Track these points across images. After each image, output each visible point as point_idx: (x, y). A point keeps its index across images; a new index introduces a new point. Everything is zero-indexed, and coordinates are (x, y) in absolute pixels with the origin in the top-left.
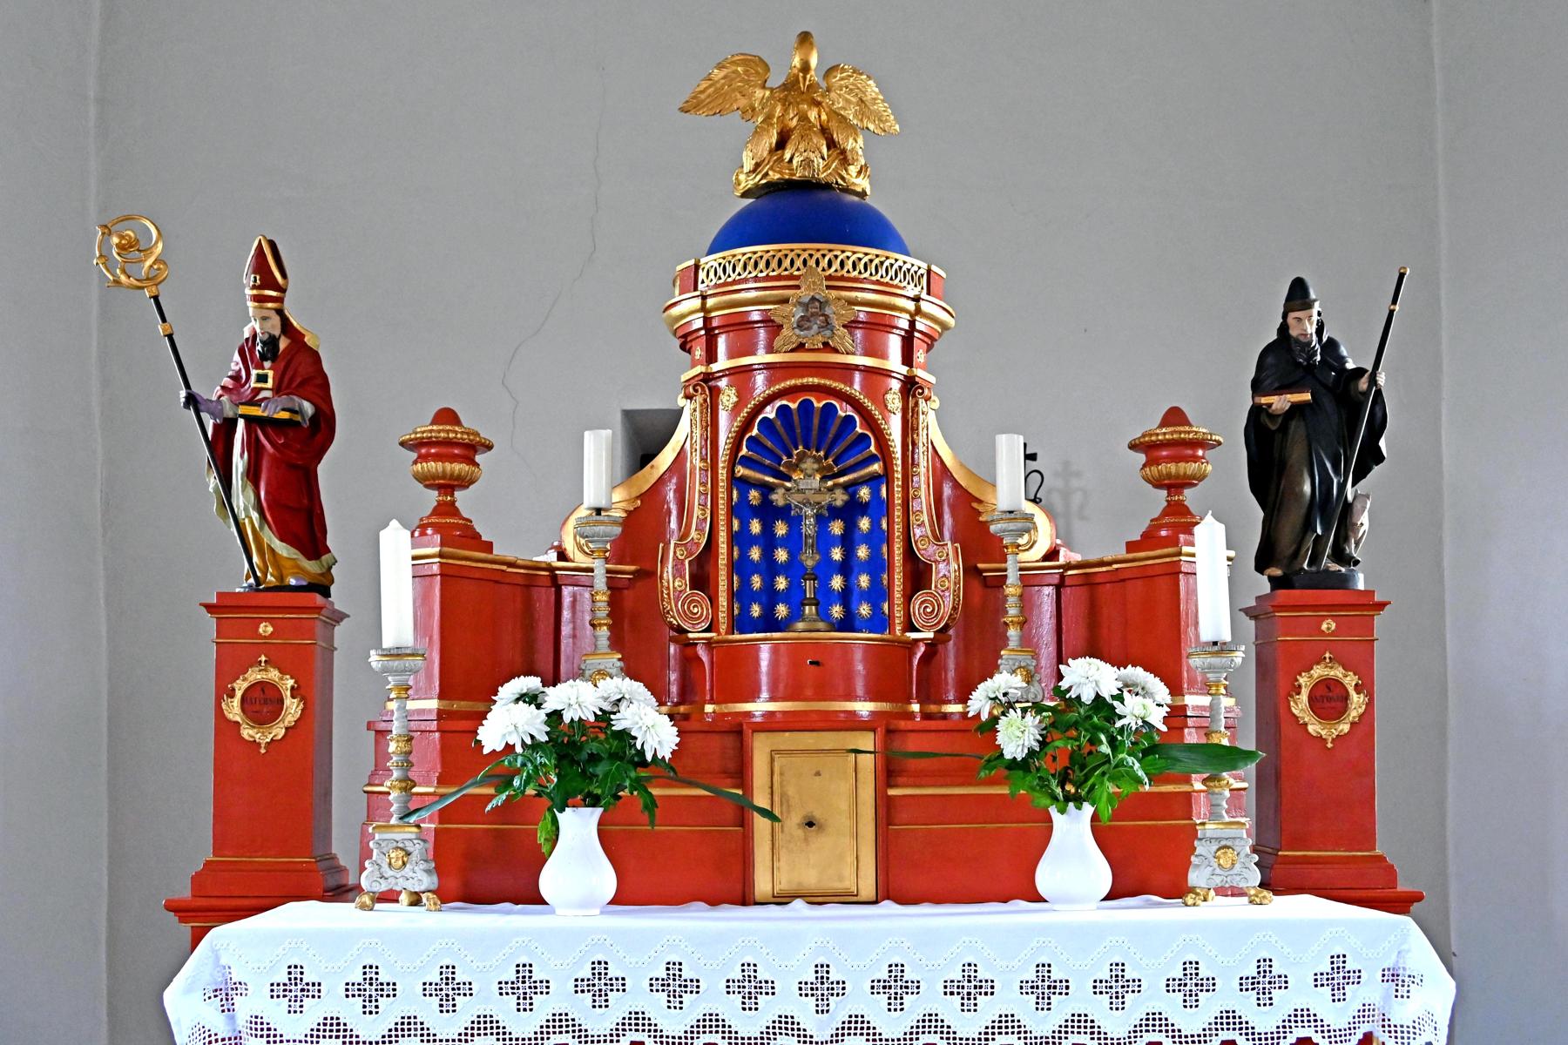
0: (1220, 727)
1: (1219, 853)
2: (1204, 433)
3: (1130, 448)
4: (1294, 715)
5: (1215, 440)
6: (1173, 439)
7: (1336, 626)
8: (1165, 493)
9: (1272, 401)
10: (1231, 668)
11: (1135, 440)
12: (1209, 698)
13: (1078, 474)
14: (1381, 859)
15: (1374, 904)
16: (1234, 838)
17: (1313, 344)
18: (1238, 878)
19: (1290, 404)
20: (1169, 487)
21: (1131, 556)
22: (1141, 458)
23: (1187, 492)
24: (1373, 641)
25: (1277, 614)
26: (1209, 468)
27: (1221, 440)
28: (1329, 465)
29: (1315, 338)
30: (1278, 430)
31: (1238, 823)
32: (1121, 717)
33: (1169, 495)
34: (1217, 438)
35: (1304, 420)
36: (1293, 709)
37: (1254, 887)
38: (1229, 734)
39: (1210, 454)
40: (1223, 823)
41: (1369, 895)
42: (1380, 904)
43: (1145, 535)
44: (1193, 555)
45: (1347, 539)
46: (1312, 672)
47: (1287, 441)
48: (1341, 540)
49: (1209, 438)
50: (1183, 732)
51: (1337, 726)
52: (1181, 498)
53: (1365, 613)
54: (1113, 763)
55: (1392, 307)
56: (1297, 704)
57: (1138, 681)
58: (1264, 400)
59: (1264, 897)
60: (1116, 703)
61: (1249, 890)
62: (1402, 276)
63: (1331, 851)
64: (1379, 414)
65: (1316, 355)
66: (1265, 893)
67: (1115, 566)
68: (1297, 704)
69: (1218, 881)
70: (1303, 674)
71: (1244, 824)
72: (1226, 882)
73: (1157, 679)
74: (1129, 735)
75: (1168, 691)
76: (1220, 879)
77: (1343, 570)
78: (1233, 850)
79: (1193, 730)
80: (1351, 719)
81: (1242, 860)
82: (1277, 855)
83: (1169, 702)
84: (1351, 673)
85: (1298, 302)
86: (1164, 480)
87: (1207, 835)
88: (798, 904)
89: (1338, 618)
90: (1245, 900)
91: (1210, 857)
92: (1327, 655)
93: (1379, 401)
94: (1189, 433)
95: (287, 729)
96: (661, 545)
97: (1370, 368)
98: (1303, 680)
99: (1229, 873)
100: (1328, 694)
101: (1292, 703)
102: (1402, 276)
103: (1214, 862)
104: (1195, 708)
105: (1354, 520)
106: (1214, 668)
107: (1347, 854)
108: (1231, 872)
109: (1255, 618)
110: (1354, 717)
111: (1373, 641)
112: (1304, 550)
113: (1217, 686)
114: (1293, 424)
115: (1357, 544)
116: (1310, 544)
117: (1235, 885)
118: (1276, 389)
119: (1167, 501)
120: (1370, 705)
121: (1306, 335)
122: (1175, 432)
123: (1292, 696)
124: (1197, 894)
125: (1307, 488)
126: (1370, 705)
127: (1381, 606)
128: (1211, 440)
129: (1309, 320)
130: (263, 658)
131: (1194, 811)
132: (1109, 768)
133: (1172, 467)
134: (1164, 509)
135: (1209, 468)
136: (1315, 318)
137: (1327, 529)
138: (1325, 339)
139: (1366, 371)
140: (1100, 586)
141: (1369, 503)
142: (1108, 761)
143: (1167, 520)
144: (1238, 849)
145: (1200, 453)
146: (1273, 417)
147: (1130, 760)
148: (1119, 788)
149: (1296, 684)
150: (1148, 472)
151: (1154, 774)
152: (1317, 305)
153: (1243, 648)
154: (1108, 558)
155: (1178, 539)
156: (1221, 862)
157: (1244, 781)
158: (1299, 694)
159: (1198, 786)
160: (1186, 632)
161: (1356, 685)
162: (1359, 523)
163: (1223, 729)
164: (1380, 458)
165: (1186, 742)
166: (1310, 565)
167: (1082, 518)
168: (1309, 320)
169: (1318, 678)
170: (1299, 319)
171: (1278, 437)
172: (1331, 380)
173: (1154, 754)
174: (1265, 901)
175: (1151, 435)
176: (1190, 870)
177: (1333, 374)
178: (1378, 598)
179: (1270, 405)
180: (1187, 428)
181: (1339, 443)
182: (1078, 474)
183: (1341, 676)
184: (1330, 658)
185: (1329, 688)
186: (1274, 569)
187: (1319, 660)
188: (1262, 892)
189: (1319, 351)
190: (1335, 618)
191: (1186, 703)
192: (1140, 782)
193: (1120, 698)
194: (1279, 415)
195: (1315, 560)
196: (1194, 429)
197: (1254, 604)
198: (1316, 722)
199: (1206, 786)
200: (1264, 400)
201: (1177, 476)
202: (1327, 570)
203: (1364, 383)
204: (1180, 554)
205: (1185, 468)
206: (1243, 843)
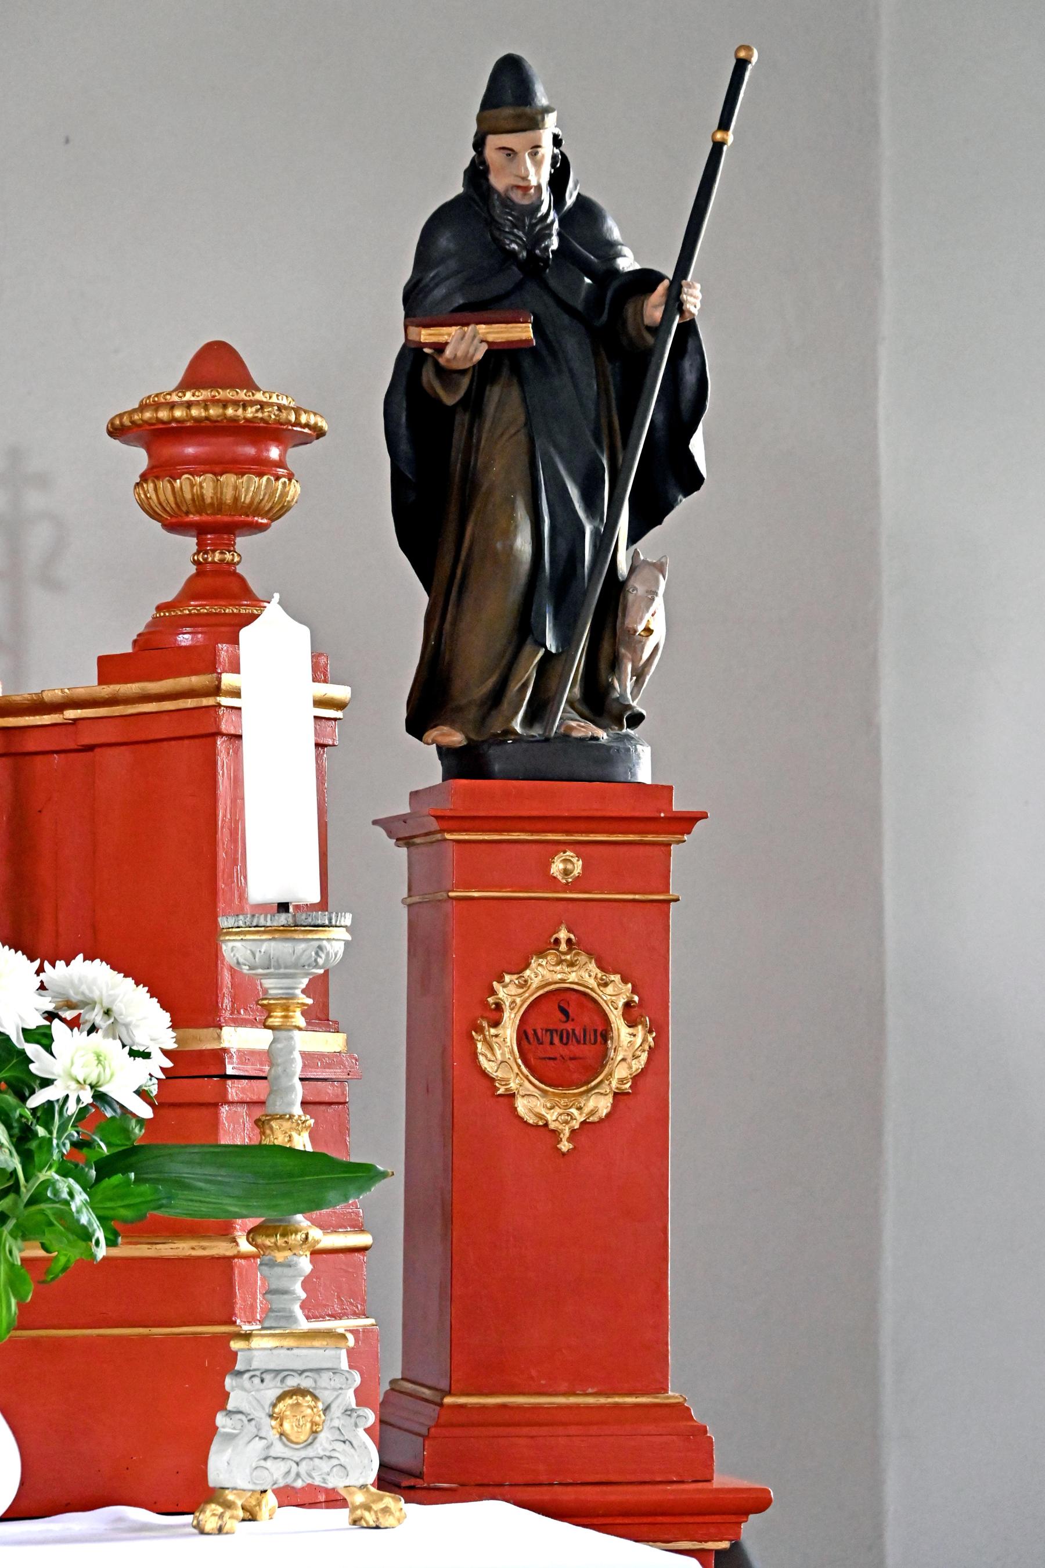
0: (291, 1104)
1: (281, 1406)
2: (280, 408)
3: (111, 434)
4: (484, 1074)
5: (307, 425)
6: (207, 418)
7: (584, 867)
8: (190, 543)
9: (442, 339)
10: (317, 965)
11: (120, 416)
12: (268, 1035)
13: (43, 481)
14: (680, 1411)
15: (595, 1521)
16: (318, 1371)
17: (544, 209)
18: (325, 1466)
19: (484, 348)
20: (200, 530)
21: (107, 690)
22: (139, 458)
23: (242, 542)
24: (668, 902)
25: (448, 836)
26: (294, 490)
27: (322, 423)
28: (574, 492)
29: (546, 196)
30: (463, 403)
31: (329, 1334)
32: (46, 1083)
33: (201, 548)
34: (313, 420)
35: (522, 384)
36: (481, 1058)
37: (363, 1487)
38: (311, 1122)
39: (296, 456)
40: (292, 1335)
41: (612, 1498)
42: (610, 1520)
43: (142, 643)
44: (236, 693)
45: (615, 665)
46: (527, 973)
47: (480, 431)
48: (603, 665)
49: (293, 418)
50: (216, 1117)
51: (582, 1101)
52: (228, 556)
53: (650, 838)
54: (26, 1194)
55: (719, 136)
56: (491, 1049)
57: (96, 995)
58: (426, 335)
59: (386, 1510)
60: (32, 1050)
61: (351, 1494)
62: (741, 65)
63: (565, 1394)
64: (690, 378)
65: (550, 235)
66: (389, 1500)
67: (71, 714)
68: (491, 1049)
69: (277, 1473)
70: (507, 978)
71: (343, 1336)
72: (298, 1475)
73: (143, 990)
74: (62, 1129)
75: (166, 1017)
76: (283, 1467)
77: (603, 735)
78: (315, 1398)
79: (242, 1110)
80: (614, 1084)
81: (336, 1423)
82: (441, 1405)
83: (171, 1045)
84: (617, 978)
85: (508, 111)
86: (187, 513)
87: (255, 1365)
88: (278, 1460)
89: (589, 849)
90: (341, 1516)
91: (261, 1415)
92: (563, 935)
93: (691, 345)
94: (245, 405)
95: (615, 1094)
96: (558, 165)
97: (669, 272)
98: (507, 992)
99: (303, 1453)
100: (563, 1026)
101: (479, 1045)
102: (741, 65)
103: (269, 1427)
104: (245, 1056)
105: (629, 623)
106: (278, 967)
107: (603, 1400)
108: (310, 1452)
109: (406, 841)
110: (621, 1081)
111: (668, 902)
112: (514, 687)
113: (286, 1008)
114: (494, 394)
115: (639, 675)
116: (532, 673)
117: (318, 1482)
118: (460, 309)
119: (196, 563)
120: (658, 1052)
121: (526, 189)
122: (215, 402)
123: (480, 1030)
124: (228, 1505)
125: (523, 544)
126: (658, 1052)
127: (687, 822)
128: (298, 424)
129: (534, 154)
130: (563, 935)
131: (239, 1303)
132: (15, 1204)
133: (206, 484)
134: (191, 580)
135: (294, 490)
136: (547, 149)
137: (567, 641)
138: (570, 201)
139: (660, 278)
140: (39, 761)
141: (663, 583)
142: (15, 1188)
143: (193, 608)
144: (326, 1396)
145: (274, 453)
146: (445, 374)
147: (65, 1185)
148: (47, 1250)
149: (491, 1000)
150: (151, 494)
151: (125, 1221)
152: (551, 119)
153: (347, 920)
154: (54, 692)
155: (215, 654)
156: (287, 1426)
157: (360, 1229)
158: (496, 1024)
159: (245, 1246)
160: (231, 876)
161: (628, 1005)
162: (640, 628)
163: (297, 1110)
164: (692, 480)
165: (225, 1140)
166: (530, 720)
167: (52, 584)
168: (534, 154)
169: (538, 988)
170: (510, 153)
171: (462, 419)
172: (583, 294)
173: (125, 1171)
174: (386, 1521)
175: (157, 406)
176: (214, 1448)
177: (587, 281)
178: (679, 805)
179: (440, 348)
180: (243, 395)
181: (598, 442)
182: (43, 481)
183: (592, 983)
184: (569, 941)
185: (564, 1012)
186: (445, 729)
187: (546, 946)
188: (381, 1499)
189: (556, 226)
190: (578, 847)
191: (224, 1044)
192: (86, 1235)
193: (42, 1037)
194: (463, 372)
195: (539, 711)
196: (259, 396)
197: (405, 809)
198: (537, 1093)
199: (256, 1246)
200: (426, 335)
201: (218, 506)
202: (565, 737)
203: (656, 307)
204: (216, 690)
205: (236, 488)
206: (338, 1381)
